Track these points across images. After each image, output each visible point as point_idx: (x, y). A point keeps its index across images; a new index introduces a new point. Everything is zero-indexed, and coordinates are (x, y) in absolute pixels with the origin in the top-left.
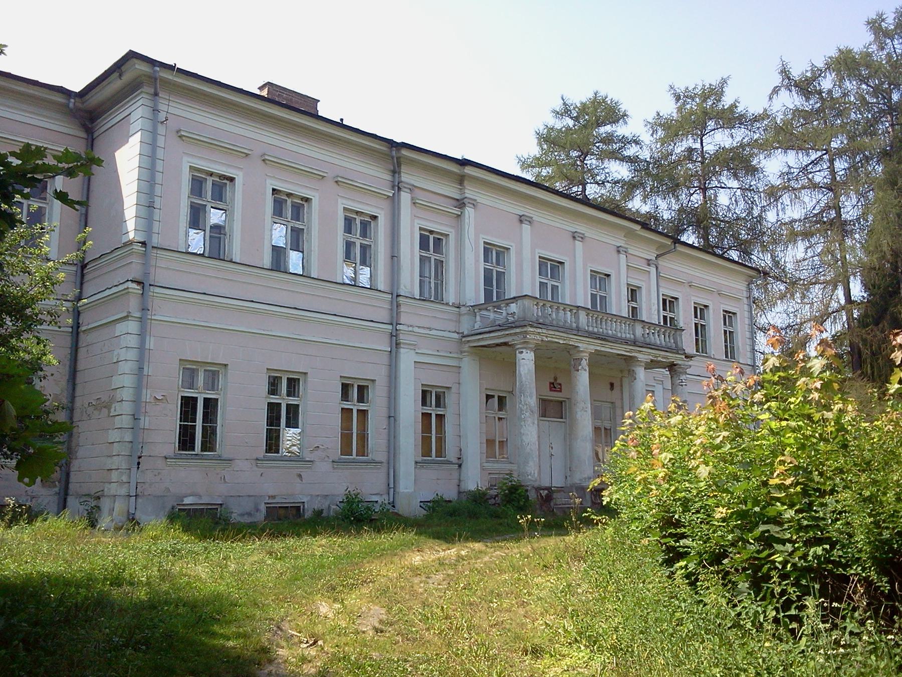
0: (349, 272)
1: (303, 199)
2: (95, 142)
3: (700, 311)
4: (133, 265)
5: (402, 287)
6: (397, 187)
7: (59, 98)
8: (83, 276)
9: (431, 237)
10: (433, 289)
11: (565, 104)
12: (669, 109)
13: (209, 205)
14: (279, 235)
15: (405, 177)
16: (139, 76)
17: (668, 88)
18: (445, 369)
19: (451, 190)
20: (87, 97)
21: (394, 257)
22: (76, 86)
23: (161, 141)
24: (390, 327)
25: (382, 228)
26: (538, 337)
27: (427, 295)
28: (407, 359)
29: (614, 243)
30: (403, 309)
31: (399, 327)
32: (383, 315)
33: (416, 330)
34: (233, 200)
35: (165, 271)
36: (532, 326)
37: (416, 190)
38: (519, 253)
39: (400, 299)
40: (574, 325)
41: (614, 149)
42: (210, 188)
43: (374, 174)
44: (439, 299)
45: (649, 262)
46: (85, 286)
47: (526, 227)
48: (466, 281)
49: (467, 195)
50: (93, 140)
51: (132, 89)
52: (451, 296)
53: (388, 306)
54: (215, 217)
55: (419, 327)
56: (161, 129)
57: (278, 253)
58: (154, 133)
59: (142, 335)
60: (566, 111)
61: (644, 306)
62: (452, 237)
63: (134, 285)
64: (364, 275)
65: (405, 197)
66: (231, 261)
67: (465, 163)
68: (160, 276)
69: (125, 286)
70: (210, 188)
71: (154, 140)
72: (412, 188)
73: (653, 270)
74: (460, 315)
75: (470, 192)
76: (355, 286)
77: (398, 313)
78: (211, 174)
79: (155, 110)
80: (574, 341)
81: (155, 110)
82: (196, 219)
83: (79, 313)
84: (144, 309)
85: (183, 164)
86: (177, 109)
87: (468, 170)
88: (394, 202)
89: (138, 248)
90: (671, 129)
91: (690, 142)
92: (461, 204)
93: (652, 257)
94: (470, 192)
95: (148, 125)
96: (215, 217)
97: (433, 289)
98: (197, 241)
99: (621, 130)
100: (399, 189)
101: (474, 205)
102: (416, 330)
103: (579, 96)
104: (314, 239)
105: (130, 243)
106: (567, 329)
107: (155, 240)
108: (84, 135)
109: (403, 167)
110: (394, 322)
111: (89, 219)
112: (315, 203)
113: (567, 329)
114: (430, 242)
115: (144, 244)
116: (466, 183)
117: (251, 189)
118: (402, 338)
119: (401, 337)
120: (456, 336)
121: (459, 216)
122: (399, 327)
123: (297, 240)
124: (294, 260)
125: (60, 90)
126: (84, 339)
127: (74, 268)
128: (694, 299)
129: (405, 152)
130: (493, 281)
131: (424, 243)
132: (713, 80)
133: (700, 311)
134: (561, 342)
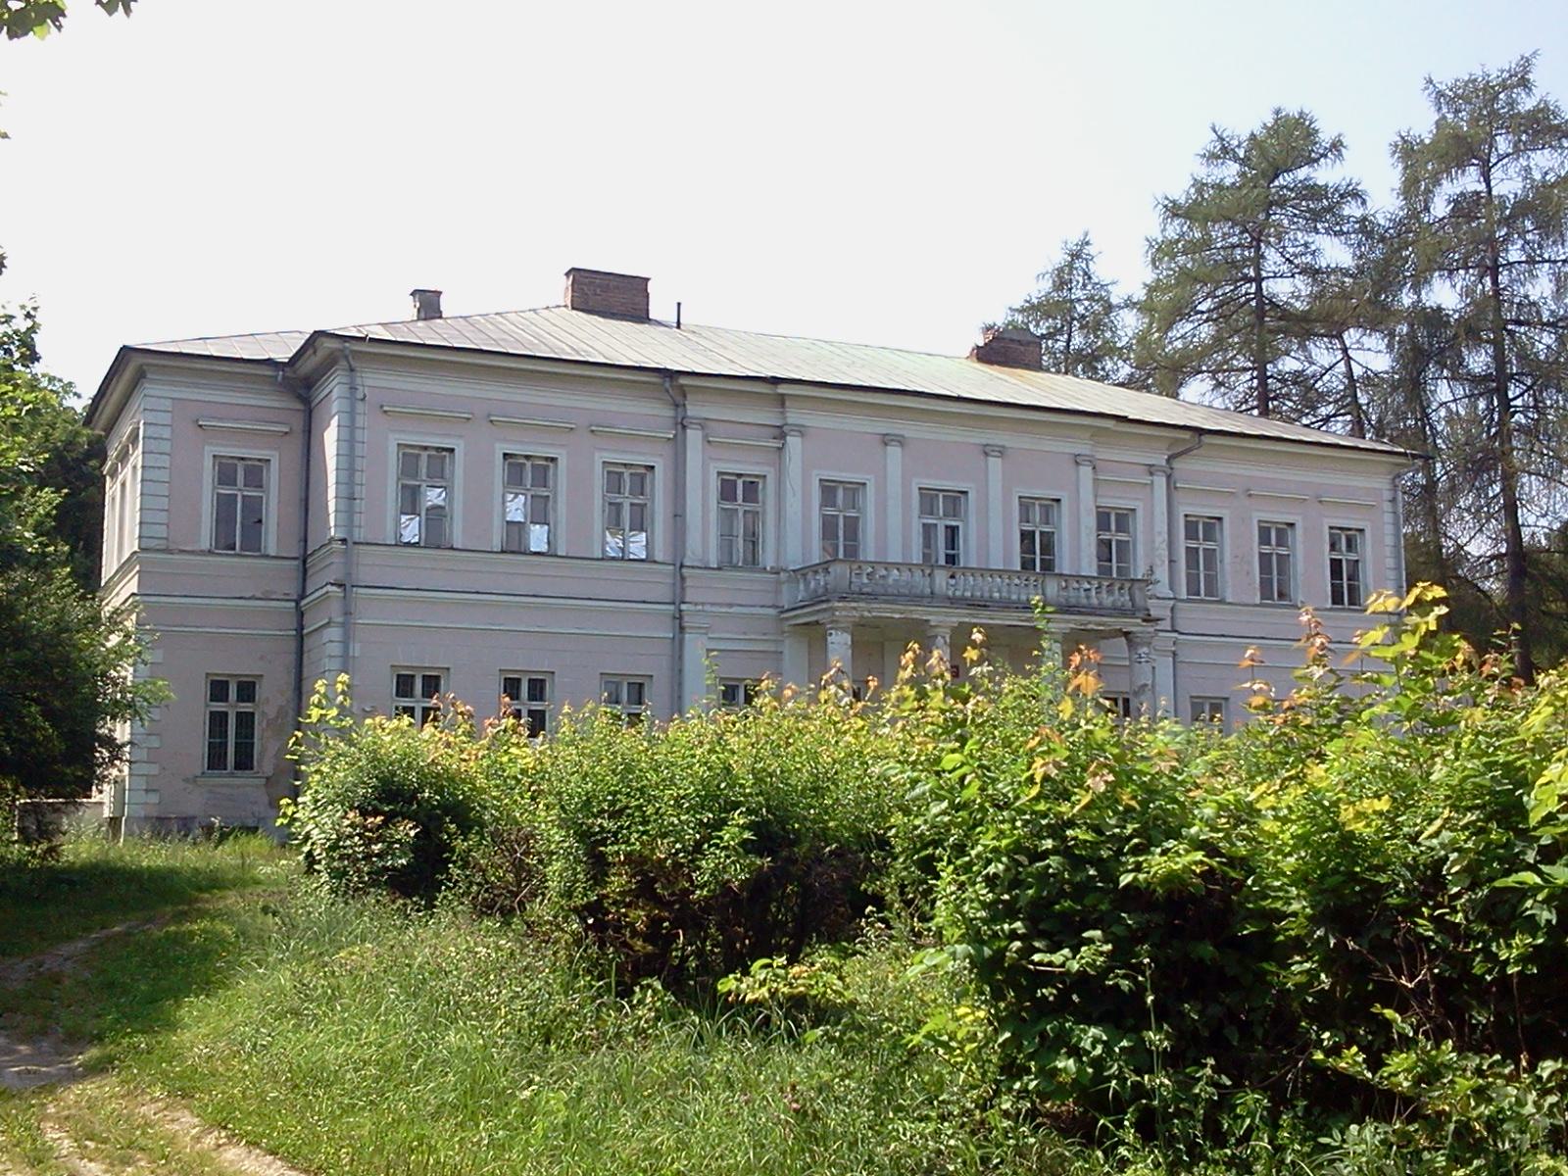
0: (613, 542)
1: (546, 459)
2: (314, 414)
3: (1275, 534)
4: (333, 567)
5: (689, 553)
6: (682, 426)
7: (268, 372)
8: (305, 571)
9: (740, 482)
10: (744, 550)
11: (1221, 139)
12: (1423, 124)
13: (424, 485)
14: (516, 508)
15: (691, 411)
16: (332, 353)
17: (1422, 84)
18: (761, 655)
19: (768, 416)
20: (299, 363)
21: (678, 516)
22: (283, 355)
23: (360, 421)
24: (672, 607)
25: (660, 480)
26: (854, 613)
27: (735, 561)
28: (695, 648)
29: (1067, 450)
30: (688, 582)
31: (684, 607)
32: (663, 592)
33: (708, 608)
34: (452, 473)
35: (370, 566)
36: (842, 599)
37: (709, 423)
38: (882, 488)
39: (684, 570)
40: (928, 591)
41: (1322, 208)
42: (425, 464)
43: (654, 412)
44: (753, 561)
45: (1151, 470)
46: (308, 581)
47: (894, 451)
48: (794, 531)
49: (790, 421)
50: (311, 412)
51: (330, 363)
52: (768, 559)
53: (669, 580)
54: (433, 497)
55: (713, 604)
56: (360, 407)
57: (516, 529)
58: (352, 414)
59: (345, 642)
60: (1224, 151)
61: (1140, 537)
62: (770, 479)
63: (334, 588)
64: (637, 545)
65: (693, 436)
66: (452, 548)
67: (776, 381)
68: (364, 575)
69: (325, 590)
70: (425, 464)
71: (353, 420)
72: (703, 424)
73: (1160, 481)
74: (779, 583)
75: (793, 416)
76: (622, 559)
77: (683, 589)
78: (426, 448)
79: (353, 389)
80: (918, 613)
81: (353, 389)
82: (410, 500)
83: (302, 614)
84: (347, 613)
85: (388, 443)
86: (373, 380)
87: (782, 389)
88: (678, 445)
89: (337, 546)
90: (1421, 163)
91: (1469, 181)
92: (781, 433)
93: (1160, 460)
94: (793, 416)
95: (345, 405)
96: (433, 497)
97: (744, 550)
98: (411, 529)
99: (1325, 174)
100: (684, 427)
101: (801, 431)
102: (708, 608)
103: (1247, 121)
104: (562, 510)
105: (332, 540)
106: (916, 598)
107: (359, 535)
108: (300, 406)
109: (689, 396)
110: (678, 600)
111: (310, 507)
112: (562, 463)
113: (916, 598)
114: (738, 490)
115: (344, 541)
116: (787, 403)
117: (476, 458)
118: (688, 621)
119: (686, 619)
120: (772, 611)
121: (780, 449)
122: (683, 607)
123: (540, 512)
124: (537, 537)
125: (269, 362)
126: (308, 643)
127: (296, 563)
128: (1257, 516)
129: (683, 381)
130: (842, 533)
131: (727, 491)
132: (1496, 63)
133: (1275, 534)
134: (897, 616)
